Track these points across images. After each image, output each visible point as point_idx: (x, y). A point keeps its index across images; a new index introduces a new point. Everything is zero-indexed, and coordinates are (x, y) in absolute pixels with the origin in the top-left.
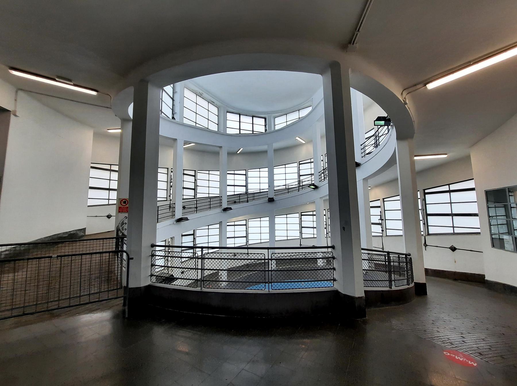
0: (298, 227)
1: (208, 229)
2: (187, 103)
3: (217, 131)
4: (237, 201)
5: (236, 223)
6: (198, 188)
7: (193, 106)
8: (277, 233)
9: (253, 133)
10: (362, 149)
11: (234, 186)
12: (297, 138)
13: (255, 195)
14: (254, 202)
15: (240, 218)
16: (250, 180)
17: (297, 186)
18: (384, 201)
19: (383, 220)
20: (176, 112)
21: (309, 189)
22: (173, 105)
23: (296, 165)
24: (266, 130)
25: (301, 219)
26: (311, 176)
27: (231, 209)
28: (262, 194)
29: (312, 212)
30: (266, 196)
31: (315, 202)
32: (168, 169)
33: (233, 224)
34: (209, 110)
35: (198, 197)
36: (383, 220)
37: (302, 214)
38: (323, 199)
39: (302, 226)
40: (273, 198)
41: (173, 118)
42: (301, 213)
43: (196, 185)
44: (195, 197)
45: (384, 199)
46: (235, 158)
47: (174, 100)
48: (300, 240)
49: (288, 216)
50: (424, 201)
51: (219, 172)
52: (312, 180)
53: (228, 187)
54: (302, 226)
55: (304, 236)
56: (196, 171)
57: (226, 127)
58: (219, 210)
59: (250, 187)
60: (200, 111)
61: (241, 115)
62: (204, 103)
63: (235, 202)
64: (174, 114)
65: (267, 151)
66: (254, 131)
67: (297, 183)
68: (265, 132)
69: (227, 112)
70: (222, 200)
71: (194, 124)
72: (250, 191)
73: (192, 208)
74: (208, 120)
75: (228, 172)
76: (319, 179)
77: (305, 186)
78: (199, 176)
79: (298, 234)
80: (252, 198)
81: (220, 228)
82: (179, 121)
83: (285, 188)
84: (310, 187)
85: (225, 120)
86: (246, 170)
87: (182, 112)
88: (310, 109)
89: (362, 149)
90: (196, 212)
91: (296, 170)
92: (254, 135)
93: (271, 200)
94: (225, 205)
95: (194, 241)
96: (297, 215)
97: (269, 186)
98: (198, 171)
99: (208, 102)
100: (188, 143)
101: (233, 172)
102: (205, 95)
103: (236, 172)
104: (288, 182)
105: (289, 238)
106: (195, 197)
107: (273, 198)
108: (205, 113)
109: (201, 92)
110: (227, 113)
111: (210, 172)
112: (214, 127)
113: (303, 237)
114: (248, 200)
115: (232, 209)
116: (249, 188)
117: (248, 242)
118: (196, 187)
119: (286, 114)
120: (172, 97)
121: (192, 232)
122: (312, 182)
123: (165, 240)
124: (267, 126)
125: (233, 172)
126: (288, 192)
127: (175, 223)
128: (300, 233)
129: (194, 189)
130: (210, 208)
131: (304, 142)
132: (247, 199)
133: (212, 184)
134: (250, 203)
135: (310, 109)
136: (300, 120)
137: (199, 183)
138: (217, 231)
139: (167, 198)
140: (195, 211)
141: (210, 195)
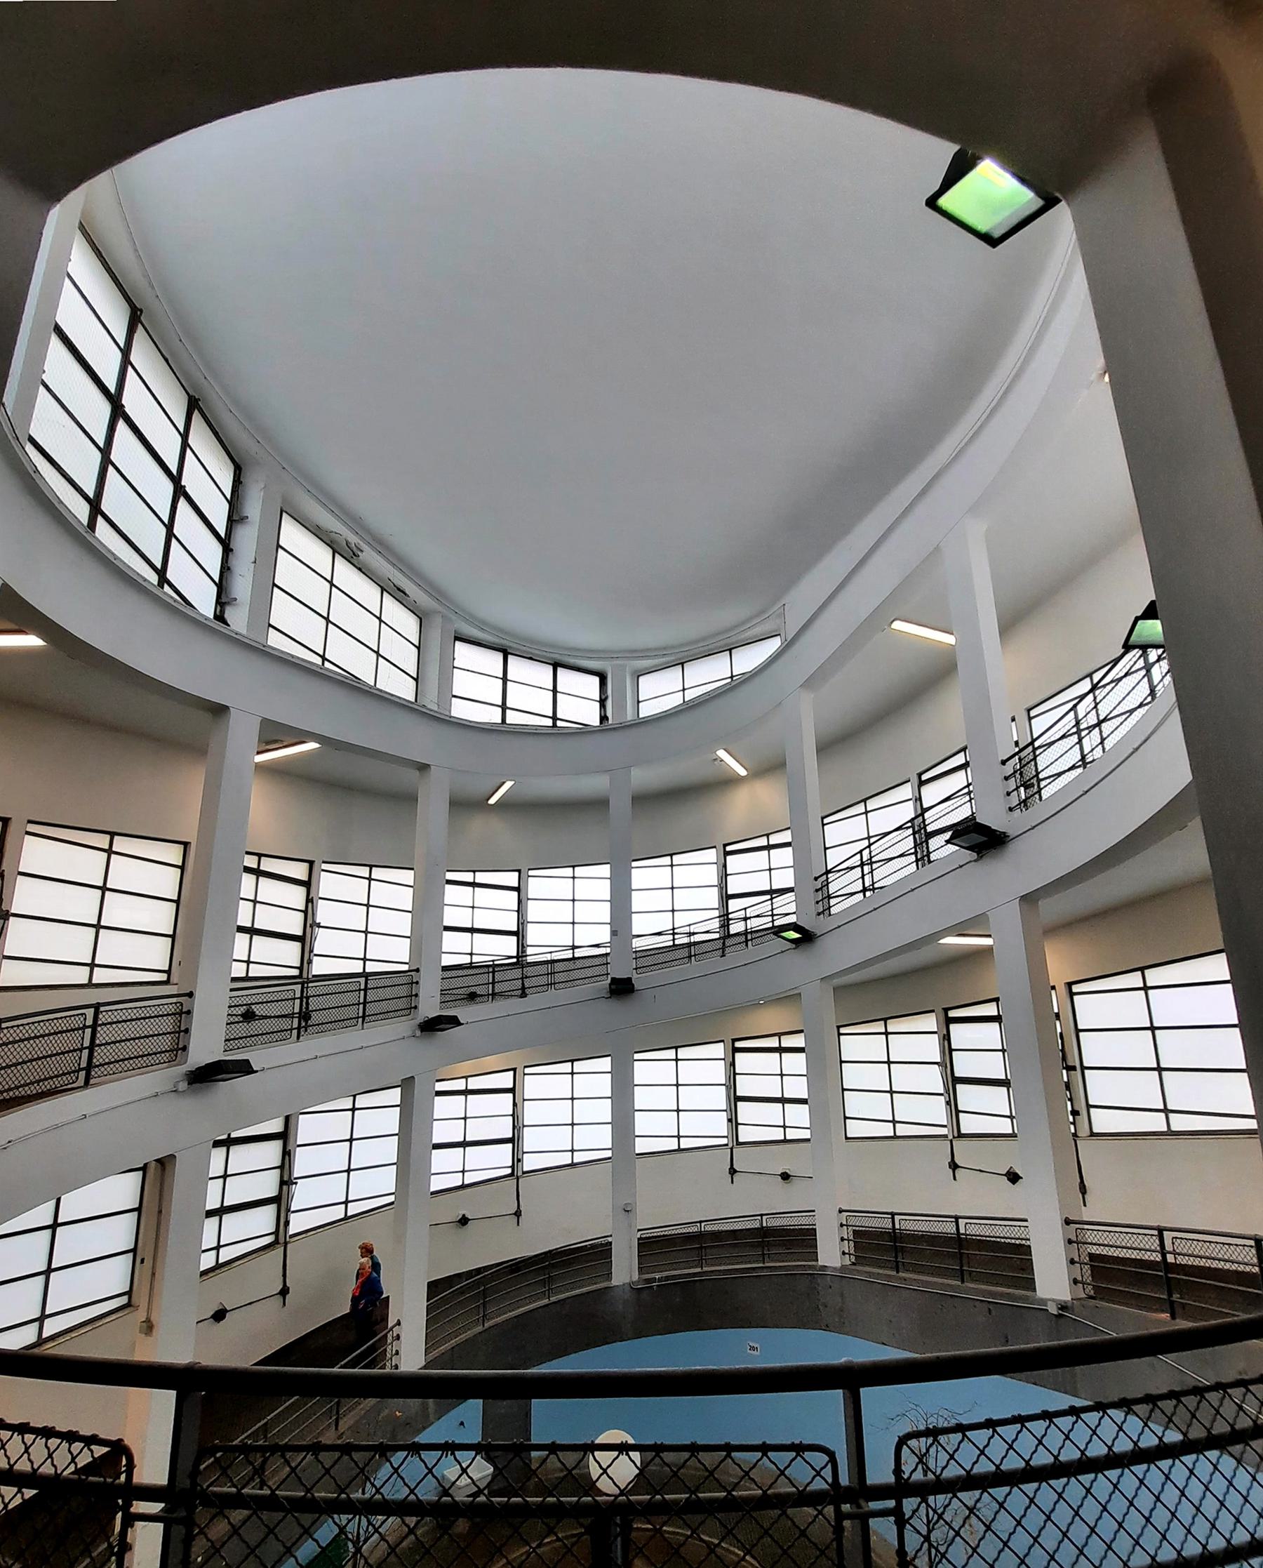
0: (719, 1098)
1: (353, 1110)
2: (287, 572)
3: (413, 700)
4: (479, 991)
5: (474, 1084)
6: (321, 933)
7: (316, 593)
8: (642, 1124)
9: (554, 725)
10: (1006, 778)
11: (472, 930)
12: (722, 754)
13: (558, 967)
14: (552, 998)
15: (491, 1061)
16: (533, 910)
17: (717, 936)
18: (1072, 994)
19: (1074, 1068)
20: (233, 597)
21: (776, 944)
22: (225, 568)
23: (711, 855)
24: (603, 718)
25: (733, 1064)
26: (769, 897)
27: (454, 1021)
28: (579, 964)
29: (777, 1038)
30: (602, 970)
31: (800, 994)
32: (186, 845)
33: (459, 1085)
34: (383, 618)
35: (315, 972)
36: (1074, 1068)
37: (738, 1044)
38: (837, 981)
39: (739, 1094)
40: (630, 979)
41: (220, 617)
42: (734, 1041)
43: (310, 921)
44: (301, 972)
45: (1070, 985)
46: (478, 826)
47: (232, 550)
48: (732, 1149)
49: (683, 1053)
50: (946, 1042)
51: (412, 872)
52: (773, 915)
53: (447, 886)
54: (739, 1094)
55: (745, 1134)
56: (316, 863)
57: (447, 693)
58: (403, 1027)
59: (534, 935)
60: (342, 611)
61: (510, 656)
62: (368, 592)
63: (472, 997)
64: (228, 603)
65: (608, 801)
66: (558, 716)
67: (715, 924)
68: (601, 723)
69: (457, 638)
70: (417, 983)
71: (318, 661)
72: (533, 954)
73: (270, 1017)
74: (377, 653)
75: (450, 876)
76: (817, 902)
77: (755, 935)
78: (328, 884)
79: (719, 1125)
80: (544, 980)
81: (405, 1108)
82: (244, 632)
83: (671, 943)
84: (783, 934)
85: (448, 667)
86: (519, 871)
87: (263, 606)
88: (774, 645)
89: (1006, 778)
90: (298, 1037)
91: (711, 875)
92: (556, 731)
93: (622, 988)
94: (430, 1007)
95: (281, 1167)
96: (718, 1050)
97: (614, 933)
98: (324, 866)
99: (383, 590)
100: (285, 744)
101: (468, 877)
102: (369, 556)
103: (481, 878)
104: (681, 920)
105: (685, 1144)
106: (301, 972)
107: (630, 979)
108: (366, 628)
109: (353, 539)
110: (457, 643)
111: (377, 873)
112: (404, 689)
113: (741, 1140)
114: (523, 988)
115: (459, 1024)
116: (530, 941)
117: (519, 1160)
118: (308, 929)
119: (682, 664)
120: (222, 534)
121: (275, 1126)
122: (773, 921)
123: (141, 1165)
124: (609, 704)
125: (468, 877)
126: (690, 957)
127: (183, 1086)
128: (730, 1120)
129: (300, 939)
130: (364, 1017)
131: (743, 772)
132: (523, 984)
133: (379, 920)
134: (534, 1000)
135: (774, 645)
136: (736, 684)
137: (324, 913)
138: (390, 1121)
139: (168, 972)
140: (291, 1030)
141: (371, 967)
